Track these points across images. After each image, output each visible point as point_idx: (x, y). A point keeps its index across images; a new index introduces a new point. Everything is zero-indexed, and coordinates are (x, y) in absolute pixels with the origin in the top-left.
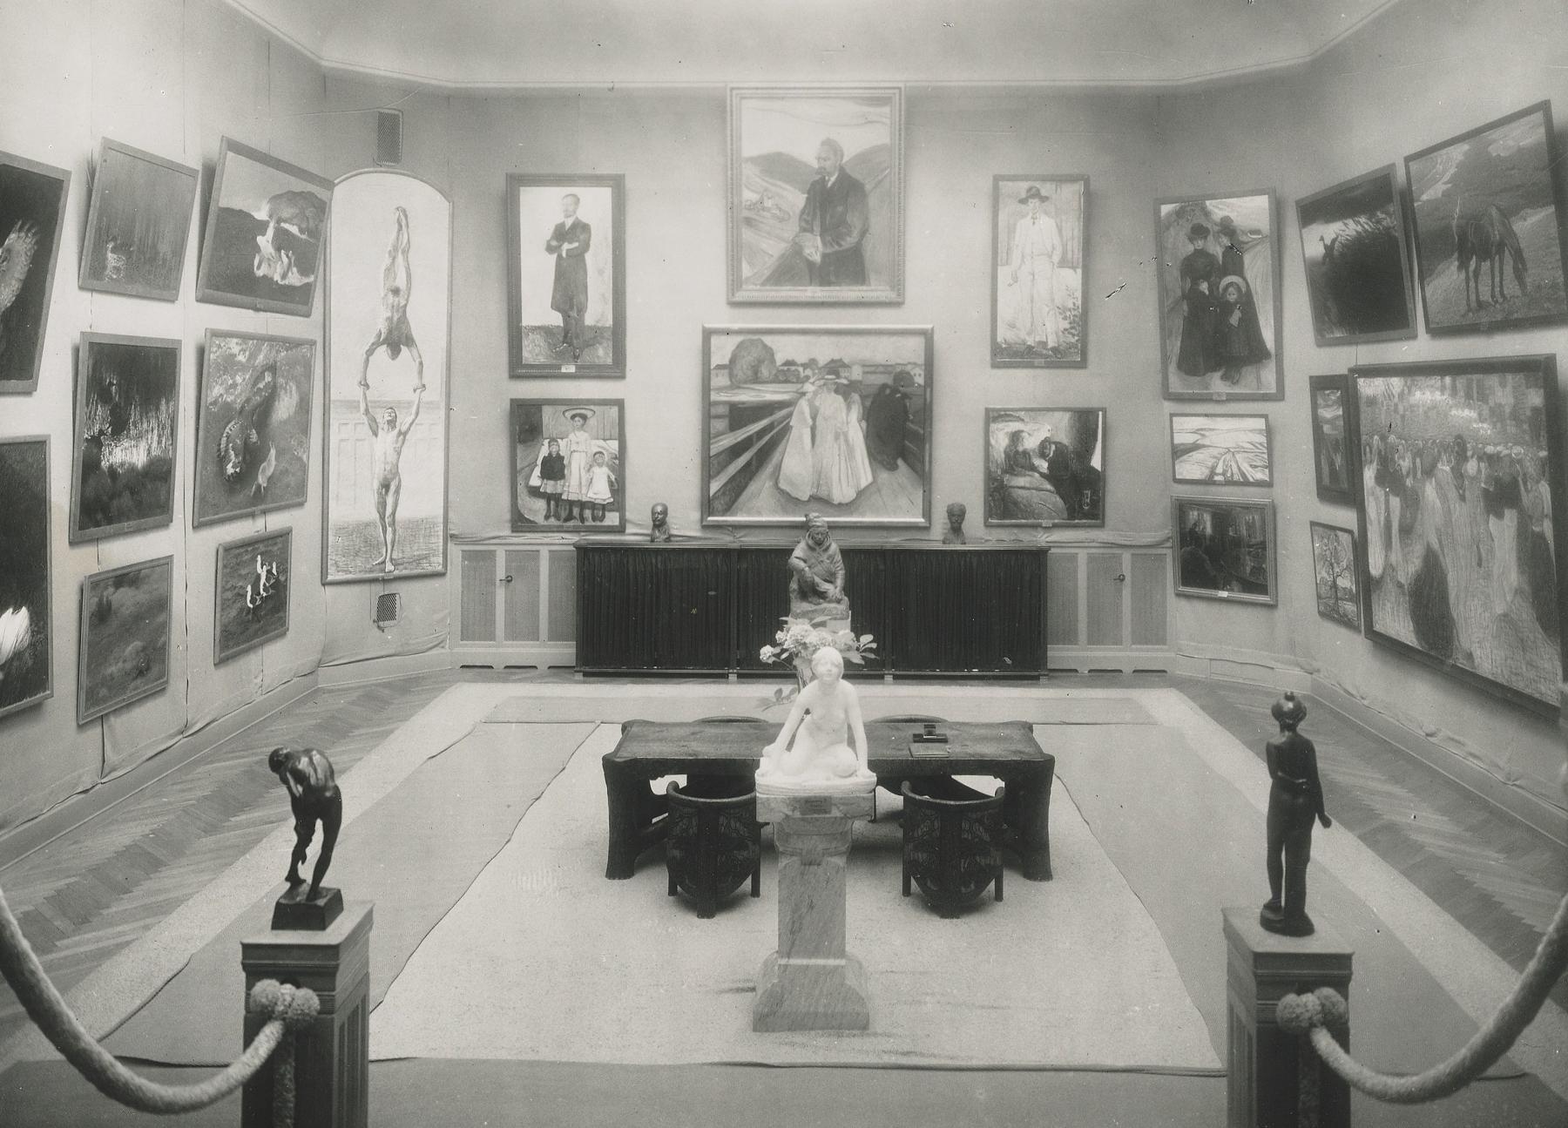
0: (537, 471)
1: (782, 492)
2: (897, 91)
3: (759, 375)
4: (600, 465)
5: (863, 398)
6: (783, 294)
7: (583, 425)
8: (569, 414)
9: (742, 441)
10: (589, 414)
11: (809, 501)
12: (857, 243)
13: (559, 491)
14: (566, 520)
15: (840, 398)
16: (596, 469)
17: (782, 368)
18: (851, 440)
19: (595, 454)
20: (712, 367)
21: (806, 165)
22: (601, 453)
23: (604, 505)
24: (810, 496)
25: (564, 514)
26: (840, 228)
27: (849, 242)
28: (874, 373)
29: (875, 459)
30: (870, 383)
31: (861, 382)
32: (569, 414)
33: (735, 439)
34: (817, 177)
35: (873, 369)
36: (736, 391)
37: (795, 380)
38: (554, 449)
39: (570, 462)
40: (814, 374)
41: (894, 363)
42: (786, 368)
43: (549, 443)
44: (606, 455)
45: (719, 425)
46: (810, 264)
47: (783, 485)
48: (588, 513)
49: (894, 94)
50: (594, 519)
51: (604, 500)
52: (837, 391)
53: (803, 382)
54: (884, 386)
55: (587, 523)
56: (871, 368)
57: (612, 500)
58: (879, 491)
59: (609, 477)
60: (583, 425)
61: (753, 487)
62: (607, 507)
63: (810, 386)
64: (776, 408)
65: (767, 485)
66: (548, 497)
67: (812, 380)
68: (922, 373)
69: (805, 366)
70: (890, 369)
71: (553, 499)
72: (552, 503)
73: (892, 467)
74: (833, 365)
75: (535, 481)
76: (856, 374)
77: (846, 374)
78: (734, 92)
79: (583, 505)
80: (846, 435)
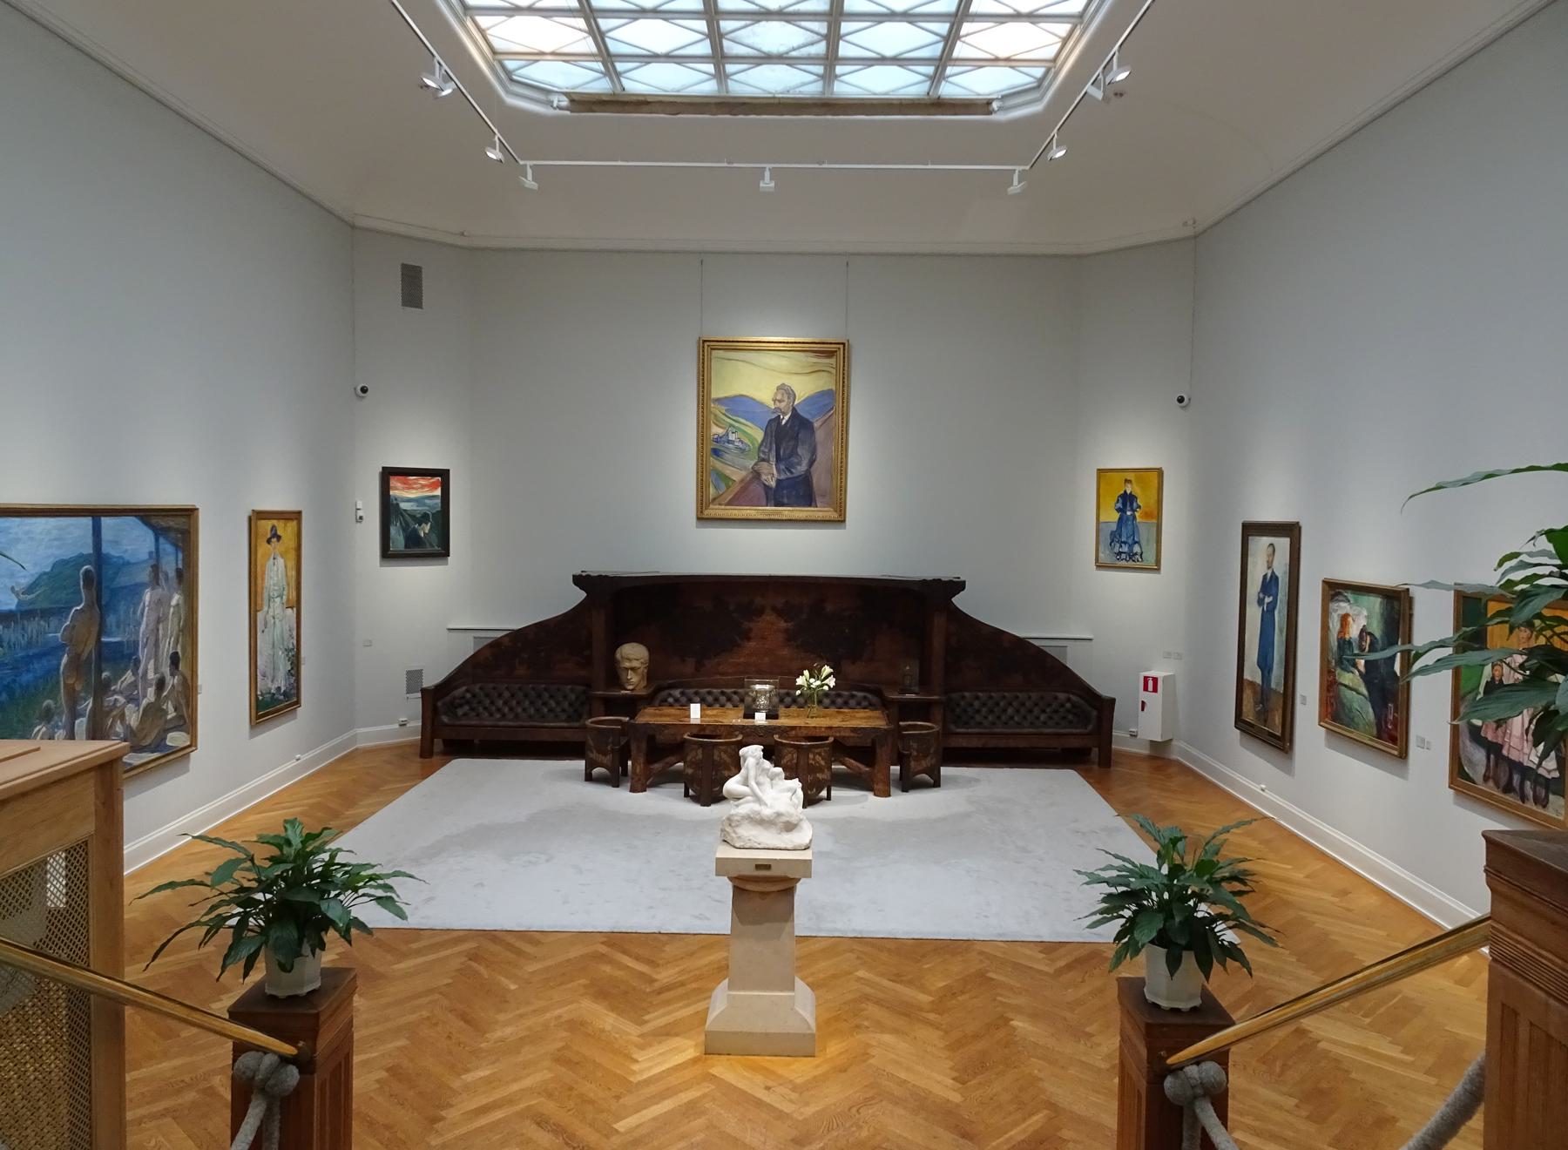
2: (841, 346)
6: (744, 512)
12: (807, 470)
21: (761, 404)
26: (792, 459)
27: (801, 469)
34: (774, 416)
46: (767, 488)
49: (839, 348)
78: (706, 344)
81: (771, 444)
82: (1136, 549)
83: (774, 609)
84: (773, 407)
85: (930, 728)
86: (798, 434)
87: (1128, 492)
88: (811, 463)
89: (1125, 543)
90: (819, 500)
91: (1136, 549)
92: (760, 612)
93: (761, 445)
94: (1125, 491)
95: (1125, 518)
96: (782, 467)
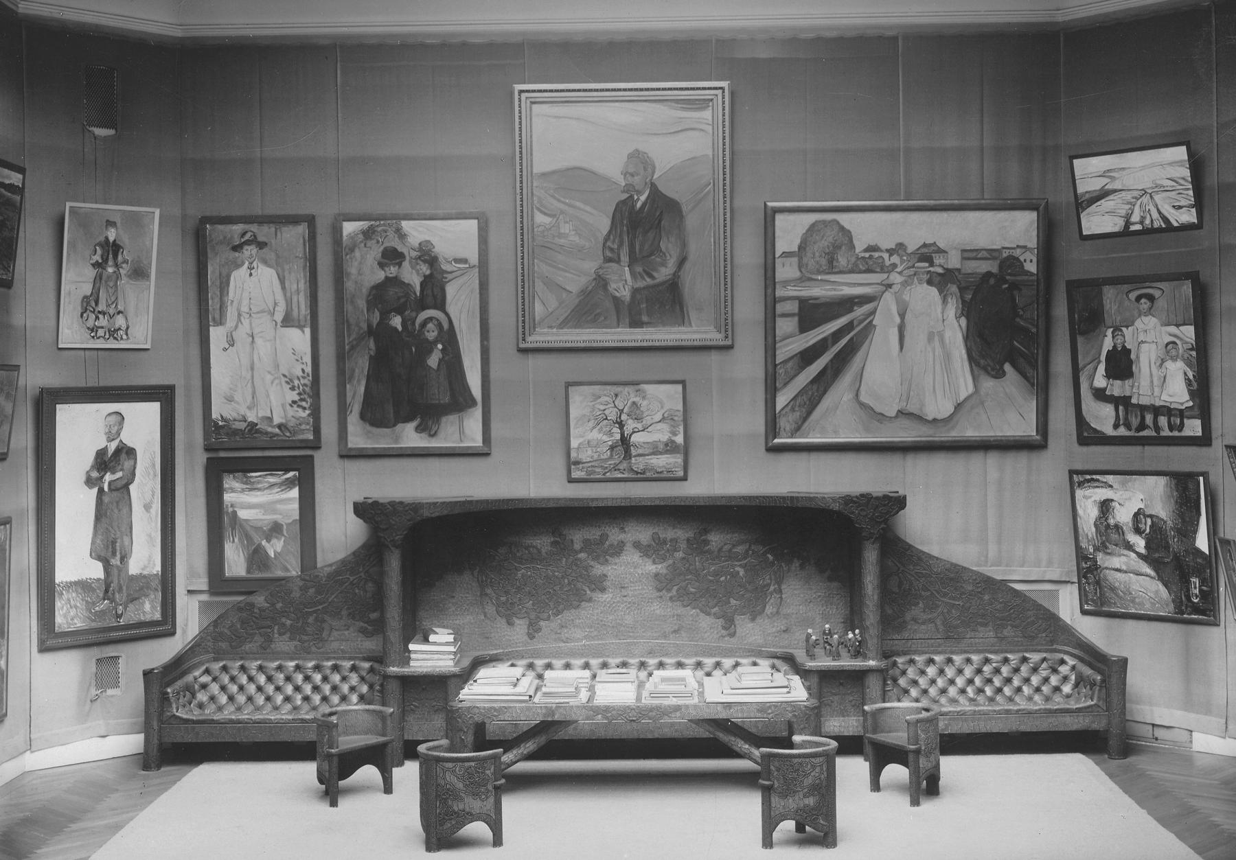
0: (1102, 369)
1: (863, 406)
3: (835, 263)
4: (1174, 359)
5: (962, 290)
7: (1150, 309)
8: (1133, 296)
9: (814, 345)
10: (1157, 293)
11: (896, 417)
12: (674, 274)
13: (1128, 394)
14: (1138, 430)
15: (934, 291)
16: (1169, 365)
17: (863, 255)
18: (947, 341)
19: (1167, 345)
20: (777, 256)
22: (1174, 343)
23: (1181, 411)
24: (899, 411)
25: (1135, 422)
27: (664, 273)
28: (976, 259)
29: (978, 365)
30: (970, 271)
31: (959, 270)
32: (1133, 296)
33: (807, 342)
35: (974, 254)
36: (807, 283)
37: (878, 270)
38: (1119, 340)
39: (1138, 357)
40: (902, 262)
41: (999, 247)
42: (867, 255)
43: (1113, 333)
44: (1180, 346)
45: (785, 326)
47: (864, 398)
48: (1163, 421)
50: (1171, 428)
51: (1182, 404)
52: (930, 282)
53: (889, 272)
54: (988, 275)
55: (1163, 434)
56: (969, 254)
57: (1191, 404)
58: (982, 403)
59: (1185, 374)
60: (1150, 309)
61: (826, 402)
62: (1186, 414)
63: (897, 275)
64: (856, 304)
65: (845, 399)
66: (1117, 401)
67: (899, 269)
68: (1035, 260)
69: (891, 252)
70: (995, 254)
71: (1122, 402)
72: (1121, 408)
73: (999, 374)
74: (925, 250)
75: (1100, 381)
76: (954, 261)
77: (942, 261)
79: (1157, 411)
80: (941, 336)
81: (621, 236)
82: (120, 321)
83: (637, 545)
84: (623, 184)
85: (818, 744)
86: (660, 222)
87: (111, 239)
88: (682, 262)
89: (104, 313)
90: (693, 315)
91: (120, 321)
92: (618, 549)
93: (606, 239)
94: (107, 238)
95: (104, 277)
96: (639, 269)
